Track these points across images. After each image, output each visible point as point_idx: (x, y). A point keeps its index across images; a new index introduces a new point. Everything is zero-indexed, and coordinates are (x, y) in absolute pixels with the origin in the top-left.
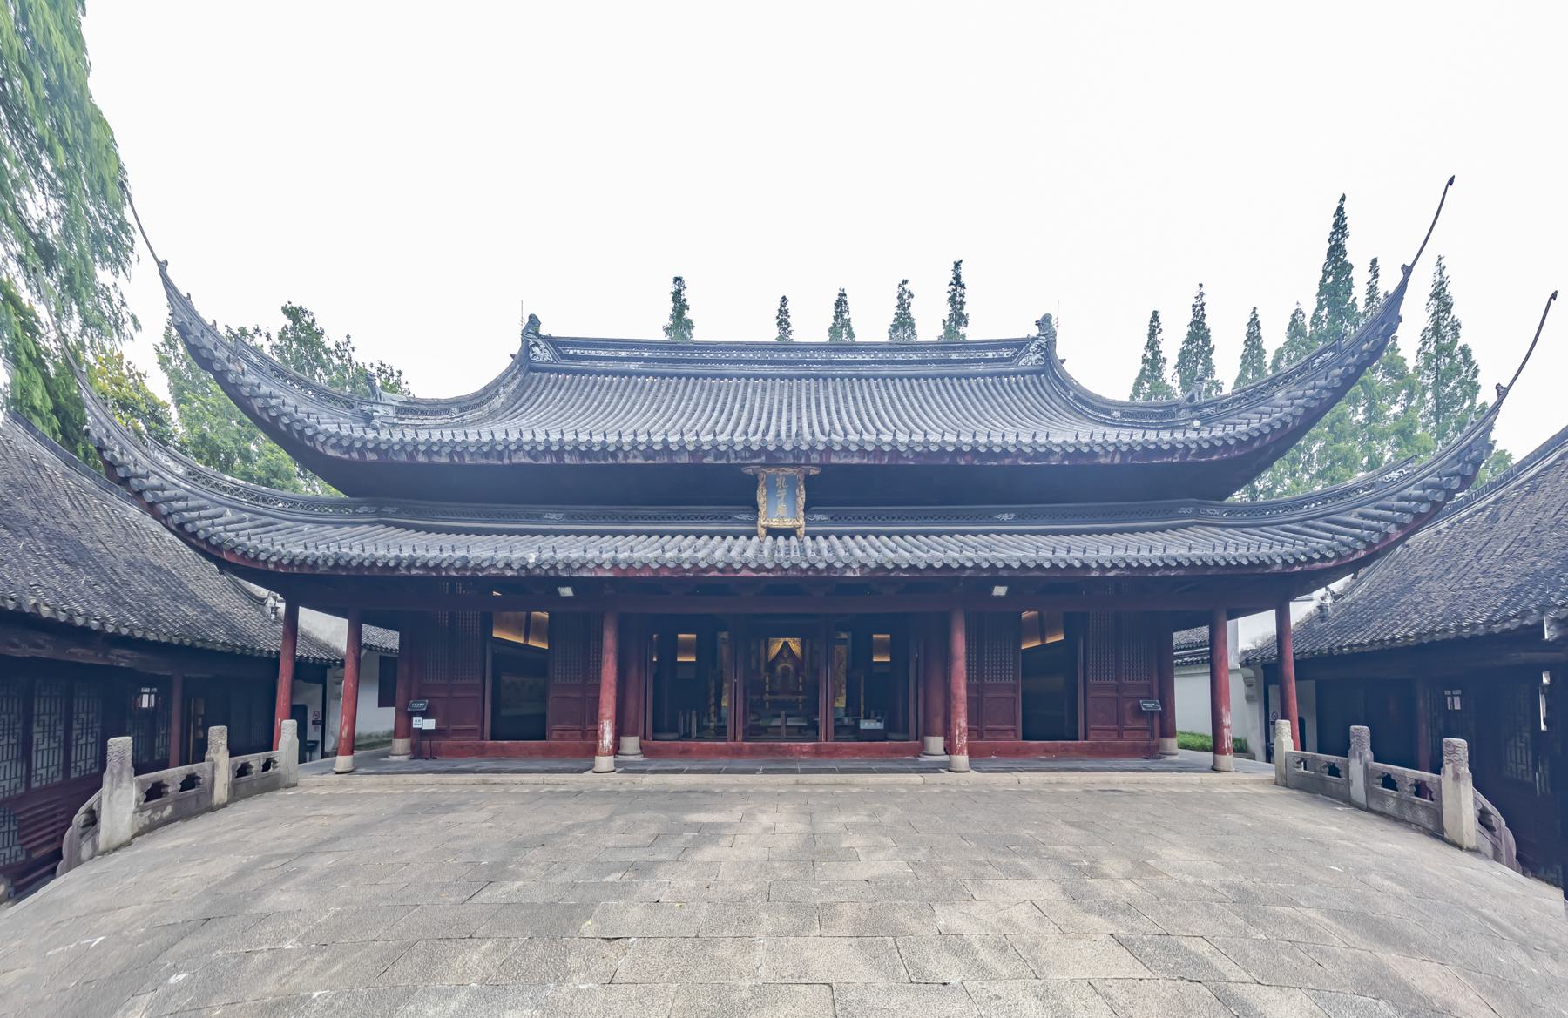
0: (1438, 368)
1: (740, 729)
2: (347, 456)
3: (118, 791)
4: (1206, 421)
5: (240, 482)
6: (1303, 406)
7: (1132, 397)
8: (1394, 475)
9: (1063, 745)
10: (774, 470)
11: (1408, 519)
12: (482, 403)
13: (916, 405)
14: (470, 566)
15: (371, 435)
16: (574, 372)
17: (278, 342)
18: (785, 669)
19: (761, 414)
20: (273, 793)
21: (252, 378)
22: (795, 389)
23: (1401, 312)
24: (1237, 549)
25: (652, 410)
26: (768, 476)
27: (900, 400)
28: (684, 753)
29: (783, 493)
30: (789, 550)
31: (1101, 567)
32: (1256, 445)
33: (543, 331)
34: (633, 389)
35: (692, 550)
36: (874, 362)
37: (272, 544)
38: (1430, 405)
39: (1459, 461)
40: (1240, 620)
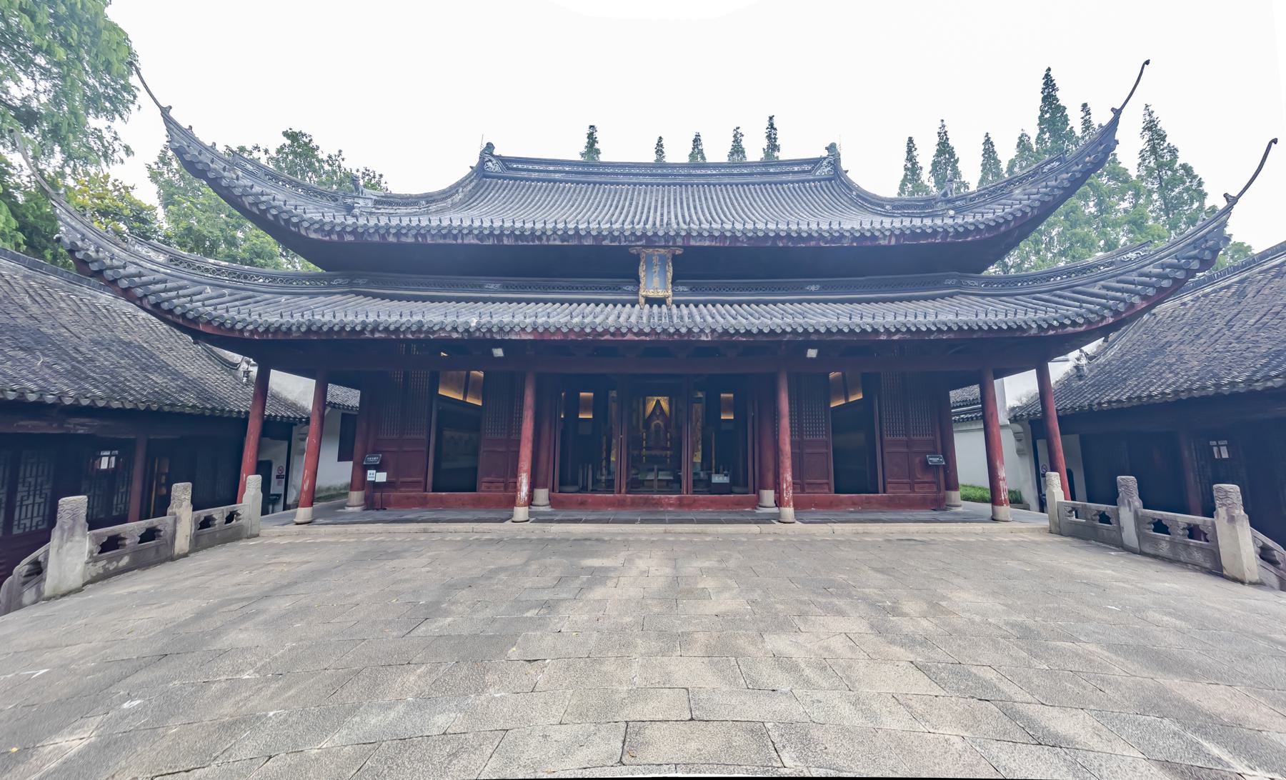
0: (1161, 178)
1: (624, 482)
2: (328, 238)
3: (69, 544)
4: (959, 210)
5: (223, 263)
6: (1039, 200)
7: (899, 194)
8: (1132, 255)
9: (867, 498)
10: (651, 250)
11: (1151, 292)
12: (447, 198)
13: (748, 203)
14: (424, 329)
15: (350, 221)
16: (516, 179)
17: (275, 155)
18: (657, 426)
19: (643, 209)
20: (236, 543)
21: (247, 182)
22: (666, 192)
23: (1117, 137)
24: (996, 316)
25: (569, 205)
26: (647, 254)
27: (737, 199)
28: (582, 504)
29: (657, 269)
30: (661, 317)
31: (887, 331)
32: (1003, 229)
33: (496, 153)
34: (556, 191)
35: (592, 316)
36: (719, 175)
37: (250, 315)
38: (1158, 204)
39: (1195, 248)
40: (1006, 379)
